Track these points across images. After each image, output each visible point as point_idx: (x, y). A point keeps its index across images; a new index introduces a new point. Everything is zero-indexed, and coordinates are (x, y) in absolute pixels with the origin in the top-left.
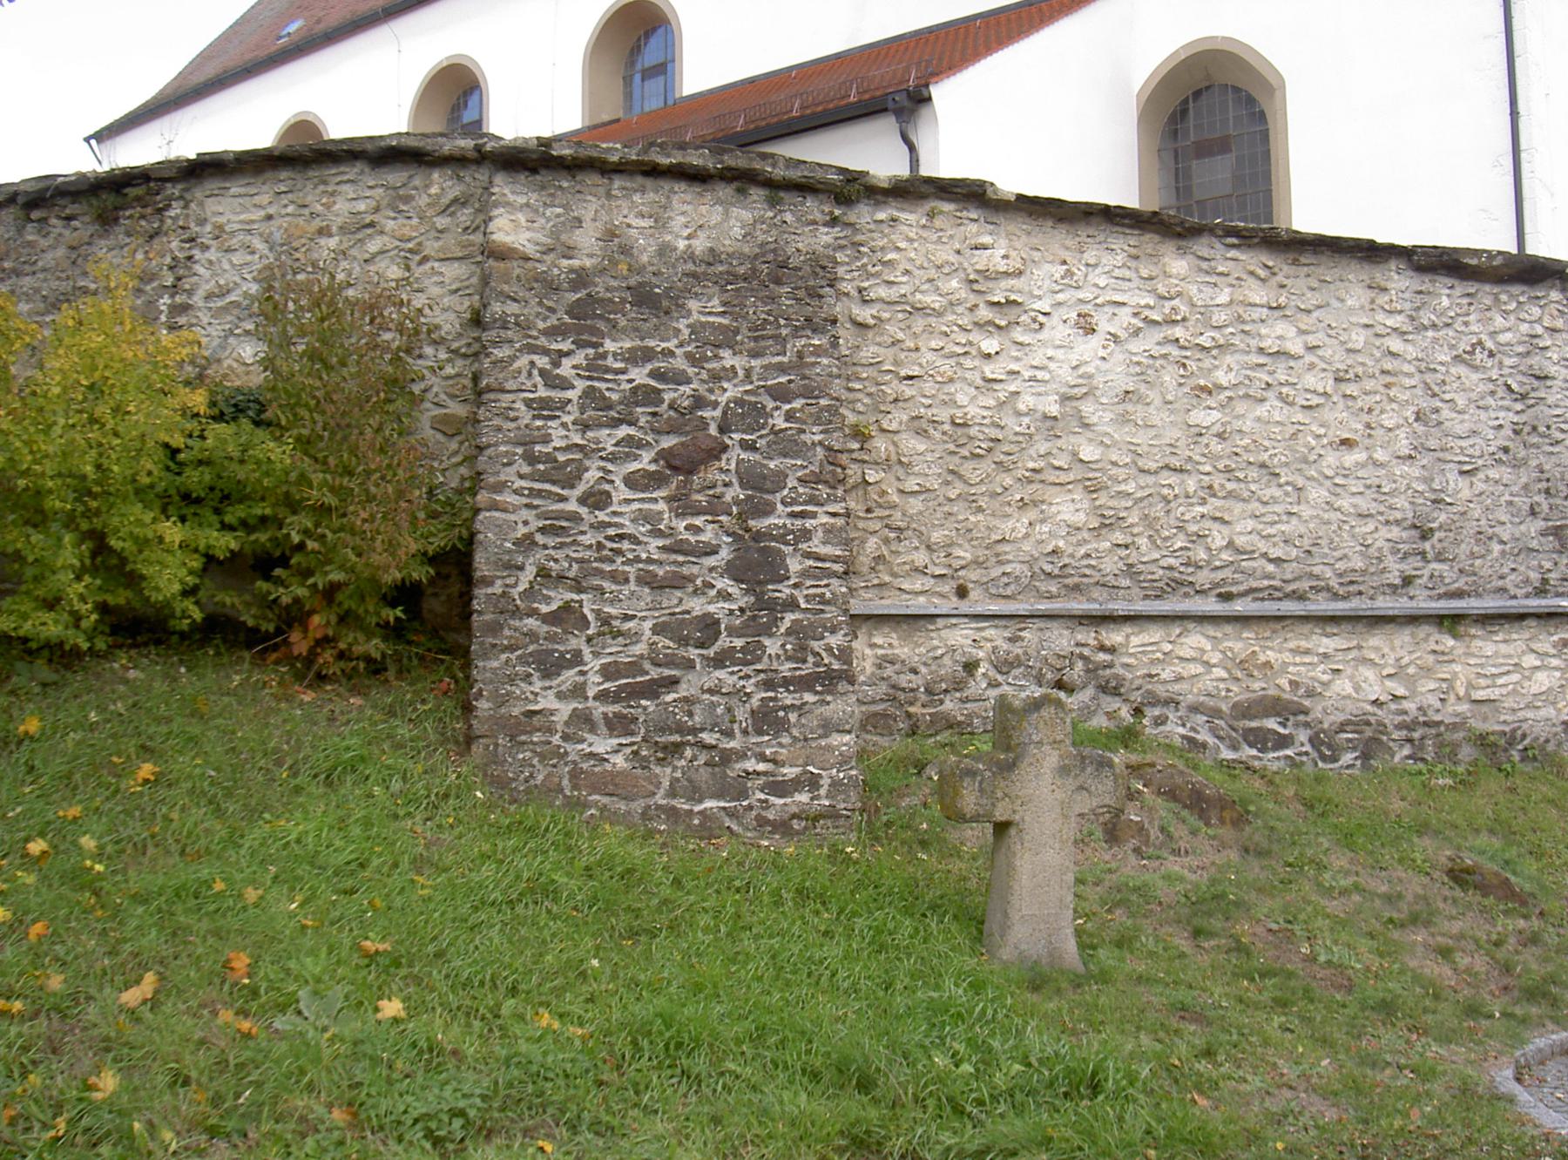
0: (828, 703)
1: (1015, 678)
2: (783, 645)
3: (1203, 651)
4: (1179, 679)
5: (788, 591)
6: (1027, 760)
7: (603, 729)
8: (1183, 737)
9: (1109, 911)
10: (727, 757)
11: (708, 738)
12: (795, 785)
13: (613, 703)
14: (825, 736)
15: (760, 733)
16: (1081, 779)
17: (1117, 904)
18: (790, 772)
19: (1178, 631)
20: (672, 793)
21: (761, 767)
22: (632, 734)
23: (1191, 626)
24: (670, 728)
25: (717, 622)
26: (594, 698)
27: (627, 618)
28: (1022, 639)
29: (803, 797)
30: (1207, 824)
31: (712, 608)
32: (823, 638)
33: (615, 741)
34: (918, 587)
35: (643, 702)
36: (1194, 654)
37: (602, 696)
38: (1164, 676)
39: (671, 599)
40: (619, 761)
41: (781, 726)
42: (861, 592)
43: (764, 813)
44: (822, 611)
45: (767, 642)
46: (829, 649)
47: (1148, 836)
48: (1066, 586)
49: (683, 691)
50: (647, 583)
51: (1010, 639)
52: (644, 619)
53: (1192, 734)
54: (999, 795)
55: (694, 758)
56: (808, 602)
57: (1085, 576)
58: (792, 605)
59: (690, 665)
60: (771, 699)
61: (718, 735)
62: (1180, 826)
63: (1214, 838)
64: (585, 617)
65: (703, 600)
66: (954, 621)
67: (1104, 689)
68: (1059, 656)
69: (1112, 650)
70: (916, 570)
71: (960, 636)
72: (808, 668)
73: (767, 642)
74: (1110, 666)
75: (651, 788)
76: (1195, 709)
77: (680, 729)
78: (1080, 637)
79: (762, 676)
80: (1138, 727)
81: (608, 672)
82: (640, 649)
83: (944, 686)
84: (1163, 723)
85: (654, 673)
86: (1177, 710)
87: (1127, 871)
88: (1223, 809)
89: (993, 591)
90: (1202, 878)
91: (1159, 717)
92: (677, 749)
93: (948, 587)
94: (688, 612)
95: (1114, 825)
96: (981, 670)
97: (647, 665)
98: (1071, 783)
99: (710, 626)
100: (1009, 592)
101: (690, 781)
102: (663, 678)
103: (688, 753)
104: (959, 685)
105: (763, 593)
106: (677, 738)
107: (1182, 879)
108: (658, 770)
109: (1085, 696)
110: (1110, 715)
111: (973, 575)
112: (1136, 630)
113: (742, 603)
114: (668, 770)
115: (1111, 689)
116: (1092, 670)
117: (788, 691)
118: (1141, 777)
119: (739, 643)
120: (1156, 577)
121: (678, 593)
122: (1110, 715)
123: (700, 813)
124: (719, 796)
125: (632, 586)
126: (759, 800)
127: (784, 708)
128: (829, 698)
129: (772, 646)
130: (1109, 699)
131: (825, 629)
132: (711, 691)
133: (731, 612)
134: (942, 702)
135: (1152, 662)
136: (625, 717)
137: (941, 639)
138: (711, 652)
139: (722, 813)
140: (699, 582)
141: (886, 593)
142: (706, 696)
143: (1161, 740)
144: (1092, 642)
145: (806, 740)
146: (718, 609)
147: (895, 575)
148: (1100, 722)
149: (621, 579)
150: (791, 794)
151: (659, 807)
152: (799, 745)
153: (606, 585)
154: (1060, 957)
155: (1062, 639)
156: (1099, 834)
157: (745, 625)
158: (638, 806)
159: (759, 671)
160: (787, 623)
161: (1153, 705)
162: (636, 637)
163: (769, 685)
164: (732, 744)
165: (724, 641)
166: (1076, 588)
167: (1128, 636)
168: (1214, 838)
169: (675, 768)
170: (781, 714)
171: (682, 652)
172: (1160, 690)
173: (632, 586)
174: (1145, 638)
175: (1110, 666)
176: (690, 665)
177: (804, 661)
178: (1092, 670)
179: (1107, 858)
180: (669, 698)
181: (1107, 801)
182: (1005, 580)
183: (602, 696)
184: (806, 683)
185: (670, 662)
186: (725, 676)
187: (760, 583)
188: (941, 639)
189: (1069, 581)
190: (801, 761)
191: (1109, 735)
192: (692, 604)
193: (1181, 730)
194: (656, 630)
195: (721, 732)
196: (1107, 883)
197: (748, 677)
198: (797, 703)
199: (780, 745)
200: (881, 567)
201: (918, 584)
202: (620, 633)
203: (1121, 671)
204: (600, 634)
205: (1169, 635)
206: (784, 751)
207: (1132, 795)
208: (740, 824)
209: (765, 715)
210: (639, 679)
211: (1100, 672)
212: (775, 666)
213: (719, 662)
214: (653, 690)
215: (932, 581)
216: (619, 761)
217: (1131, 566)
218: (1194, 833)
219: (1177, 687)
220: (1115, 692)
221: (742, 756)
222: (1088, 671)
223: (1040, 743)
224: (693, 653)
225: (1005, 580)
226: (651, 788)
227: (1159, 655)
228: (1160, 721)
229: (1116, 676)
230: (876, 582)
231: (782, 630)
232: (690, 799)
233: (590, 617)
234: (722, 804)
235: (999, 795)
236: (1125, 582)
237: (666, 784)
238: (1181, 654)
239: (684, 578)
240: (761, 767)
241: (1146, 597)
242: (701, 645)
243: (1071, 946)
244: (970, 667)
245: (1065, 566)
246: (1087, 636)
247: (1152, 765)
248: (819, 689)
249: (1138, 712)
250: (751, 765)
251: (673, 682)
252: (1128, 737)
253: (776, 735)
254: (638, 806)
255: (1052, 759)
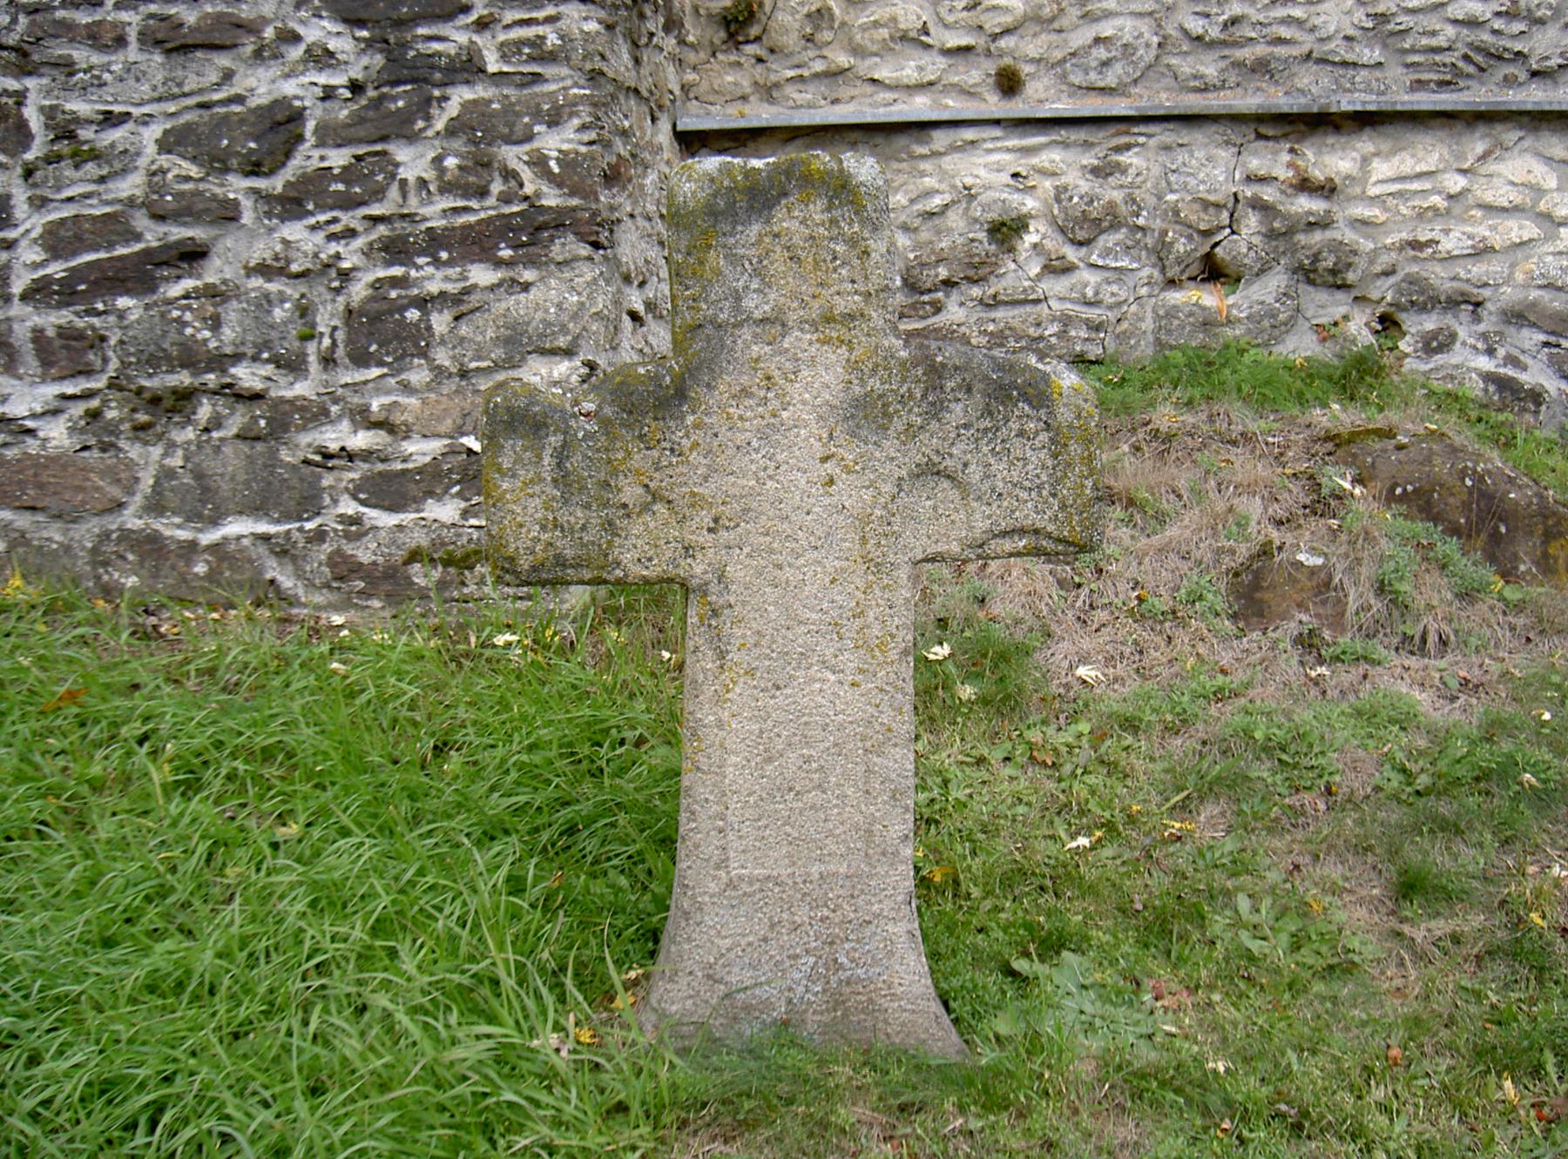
0: (526, 287)
1: (1107, 252)
2: (438, 161)
3: (1538, 191)
4: (1482, 251)
5: (462, 38)
6: (726, 384)
7: (30, 363)
8: (1488, 377)
9: (1183, 809)
10: (285, 419)
11: (247, 376)
12: (431, 480)
13: (60, 305)
14: (511, 363)
15: (361, 359)
16: (929, 443)
17: (1209, 789)
18: (420, 450)
19: (1480, 148)
20: (156, 506)
21: (361, 440)
22: (88, 372)
23: (1511, 135)
24: (168, 358)
25: (297, 116)
26: (24, 297)
27: (110, 120)
28: (1122, 169)
29: (445, 511)
30: (1508, 575)
31: (289, 88)
32: (529, 138)
33: (52, 390)
34: (909, 73)
35: (123, 302)
36: (1515, 197)
37: (38, 293)
38: (1448, 244)
39: (203, 72)
40: (57, 434)
41: (415, 343)
42: (790, 91)
43: (349, 549)
44: (537, 78)
45: (401, 152)
46: (538, 162)
47: (1341, 603)
48: (1238, 65)
49: (214, 272)
50: (158, 43)
51: (1095, 171)
52: (146, 120)
53: (1510, 372)
54: (631, 493)
55: (216, 422)
56: (504, 58)
57: (1280, 41)
58: (468, 67)
59: (228, 214)
60: (395, 282)
61: (269, 370)
62: (1433, 578)
63: (1519, 607)
64: (22, 126)
65: (275, 70)
66: (969, 134)
67: (1308, 274)
68: (1206, 205)
69: (1327, 190)
70: (904, 38)
71: (987, 169)
72: (483, 210)
73: (401, 152)
74: (1324, 223)
75: (115, 492)
76: (1517, 316)
77: (190, 357)
78: (1255, 164)
79: (382, 230)
80: (1388, 360)
81: (57, 241)
82: (130, 186)
83: (943, 272)
84: (1445, 347)
85: (153, 235)
86: (1477, 319)
87: (1267, 695)
88: (1548, 536)
89: (1077, 78)
90: (1464, 716)
91: (1434, 335)
92: (184, 399)
93: (976, 74)
94: (239, 99)
95: (1258, 576)
96: (1030, 238)
97: (141, 221)
98: (891, 456)
99: (283, 124)
100: (1110, 79)
101: (199, 476)
102: (166, 247)
103: (204, 411)
104: (977, 271)
105: (405, 46)
106: (184, 379)
107: (1405, 721)
108: (134, 451)
109: (1267, 290)
110: (1325, 333)
111: (1031, 46)
112: (1385, 146)
113: (356, 73)
114: (156, 452)
115: (1327, 274)
116: (1281, 233)
117: (437, 262)
118: (1352, 461)
119: (338, 158)
120: (1440, 41)
121: (223, 60)
122: (1325, 333)
123: (215, 548)
124: (256, 509)
125: (133, 52)
126: (343, 519)
127: (423, 303)
128: (528, 275)
129: (412, 161)
130: (1322, 296)
131: (537, 115)
132: (264, 270)
133: (329, 94)
134: (938, 308)
135: (1421, 215)
136: (79, 336)
137: (943, 174)
138: (277, 184)
139: (262, 549)
140: (269, 33)
141: (845, 92)
142: (257, 282)
143: (1436, 385)
144: (1283, 173)
145: (464, 374)
146: (299, 88)
147: (857, 51)
148: (1300, 346)
149: (107, 38)
150: (416, 502)
151: (126, 535)
152: (449, 386)
153: (81, 55)
154: (871, 1008)
155: (1211, 167)
156: (1216, 599)
157: (358, 120)
158: (86, 532)
159: (376, 220)
160: (453, 108)
161: (1423, 308)
162: (124, 160)
163: (395, 250)
164: (301, 389)
165: (307, 158)
166: (1261, 67)
167: (1365, 160)
168: (1519, 607)
169: (171, 446)
170: (413, 315)
171: (213, 187)
172: (1440, 277)
173: (133, 52)
174: (1405, 163)
175: (1324, 223)
176: (228, 214)
177: (483, 193)
178: (1281, 233)
179: (1226, 659)
180: (175, 290)
181: (1027, 515)
182: (1101, 53)
183: (38, 293)
184: (473, 243)
185: (186, 211)
186: (302, 237)
187: (400, 23)
188: (943, 174)
189: (1246, 54)
190: (447, 425)
191: (1310, 373)
192: (251, 82)
193: (1484, 363)
194: (164, 146)
195: (277, 361)
196: (1200, 730)
197: (351, 233)
198: (452, 288)
199: (406, 388)
200: (827, 35)
201: (910, 68)
202: (95, 156)
203: (1349, 236)
204: (52, 159)
205: (1461, 157)
206: (413, 401)
207: (1323, 504)
208: (299, 574)
209: (376, 318)
210: (121, 251)
211: (1301, 238)
212: (413, 204)
213: (291, 205)
214: (139, 275)
215: (942, 63)
216: (57, 434)
217: (1382, 18)
218: (1467, 595)
219: (1478, 270)
220: (1336, 281)
221: (316, 414)
222: (1271, 235)
223: (775, 322)
224: (237, 186)
225: (1101, 53)
226: (115, 492)
227: (1436, 200)
228: (1436, 344)
229: (1337, 246)
230: (819, 66)
231: (440, 125)
232: (193, 517)
233: (35, 121)
234: (263, 527)
235: (631, 493)
236: (1369, 54)
237: (147, 481)
238: (1488, 197)
239: (239, 26)
240: (361, 440)
241: (1419, 85)
242: (254, 169)
243: (905, 977)
244: (1006, 231)
245: (1234, 21)
246: (1274, 160)
247: (1388, 434)
248: (506, 253)
249: (1388, 323)
250: (337, 435)
251: (193, 255)
252: (1357, 375)
253: (397, 368)
254: (86, 532)
255: (820, 377)
